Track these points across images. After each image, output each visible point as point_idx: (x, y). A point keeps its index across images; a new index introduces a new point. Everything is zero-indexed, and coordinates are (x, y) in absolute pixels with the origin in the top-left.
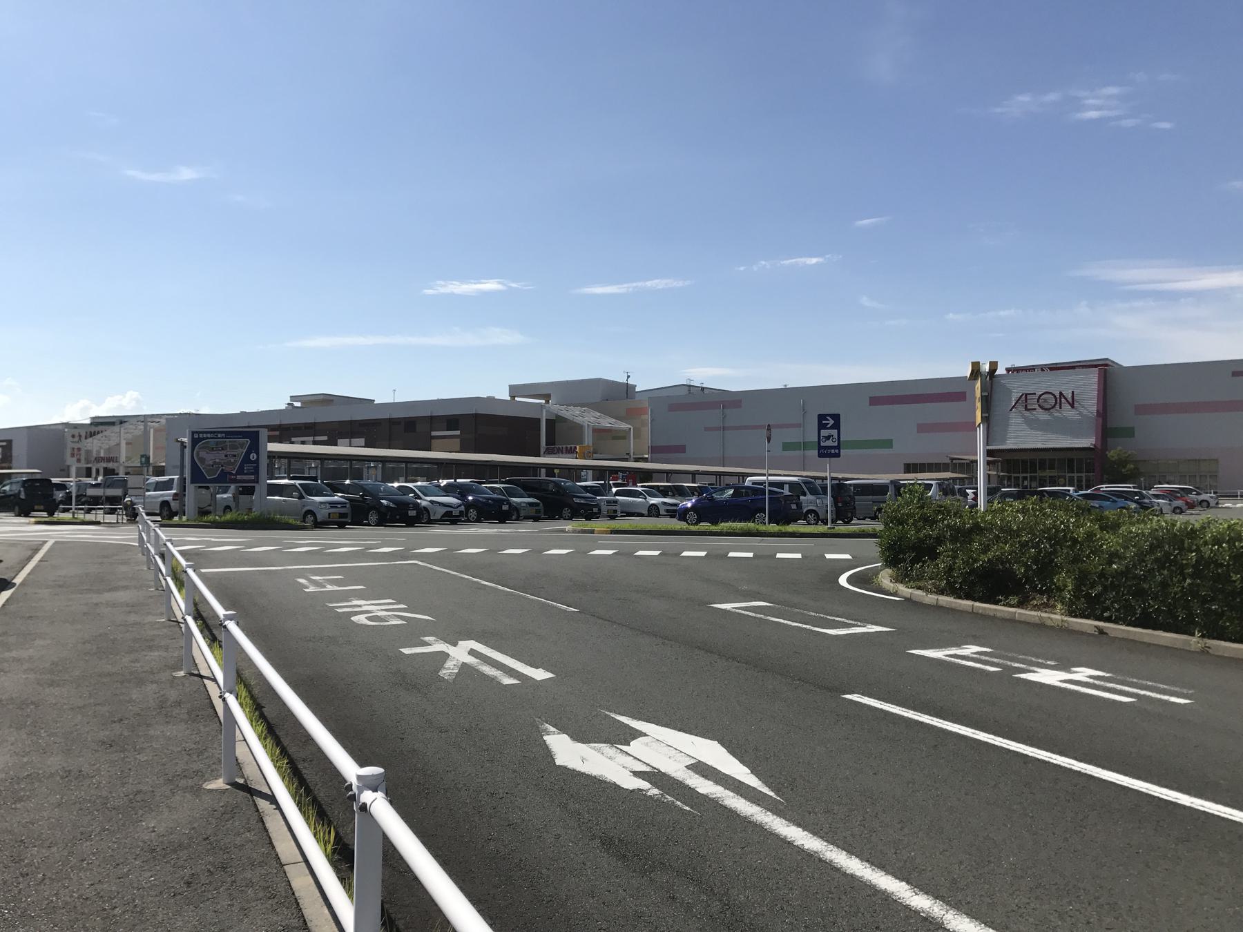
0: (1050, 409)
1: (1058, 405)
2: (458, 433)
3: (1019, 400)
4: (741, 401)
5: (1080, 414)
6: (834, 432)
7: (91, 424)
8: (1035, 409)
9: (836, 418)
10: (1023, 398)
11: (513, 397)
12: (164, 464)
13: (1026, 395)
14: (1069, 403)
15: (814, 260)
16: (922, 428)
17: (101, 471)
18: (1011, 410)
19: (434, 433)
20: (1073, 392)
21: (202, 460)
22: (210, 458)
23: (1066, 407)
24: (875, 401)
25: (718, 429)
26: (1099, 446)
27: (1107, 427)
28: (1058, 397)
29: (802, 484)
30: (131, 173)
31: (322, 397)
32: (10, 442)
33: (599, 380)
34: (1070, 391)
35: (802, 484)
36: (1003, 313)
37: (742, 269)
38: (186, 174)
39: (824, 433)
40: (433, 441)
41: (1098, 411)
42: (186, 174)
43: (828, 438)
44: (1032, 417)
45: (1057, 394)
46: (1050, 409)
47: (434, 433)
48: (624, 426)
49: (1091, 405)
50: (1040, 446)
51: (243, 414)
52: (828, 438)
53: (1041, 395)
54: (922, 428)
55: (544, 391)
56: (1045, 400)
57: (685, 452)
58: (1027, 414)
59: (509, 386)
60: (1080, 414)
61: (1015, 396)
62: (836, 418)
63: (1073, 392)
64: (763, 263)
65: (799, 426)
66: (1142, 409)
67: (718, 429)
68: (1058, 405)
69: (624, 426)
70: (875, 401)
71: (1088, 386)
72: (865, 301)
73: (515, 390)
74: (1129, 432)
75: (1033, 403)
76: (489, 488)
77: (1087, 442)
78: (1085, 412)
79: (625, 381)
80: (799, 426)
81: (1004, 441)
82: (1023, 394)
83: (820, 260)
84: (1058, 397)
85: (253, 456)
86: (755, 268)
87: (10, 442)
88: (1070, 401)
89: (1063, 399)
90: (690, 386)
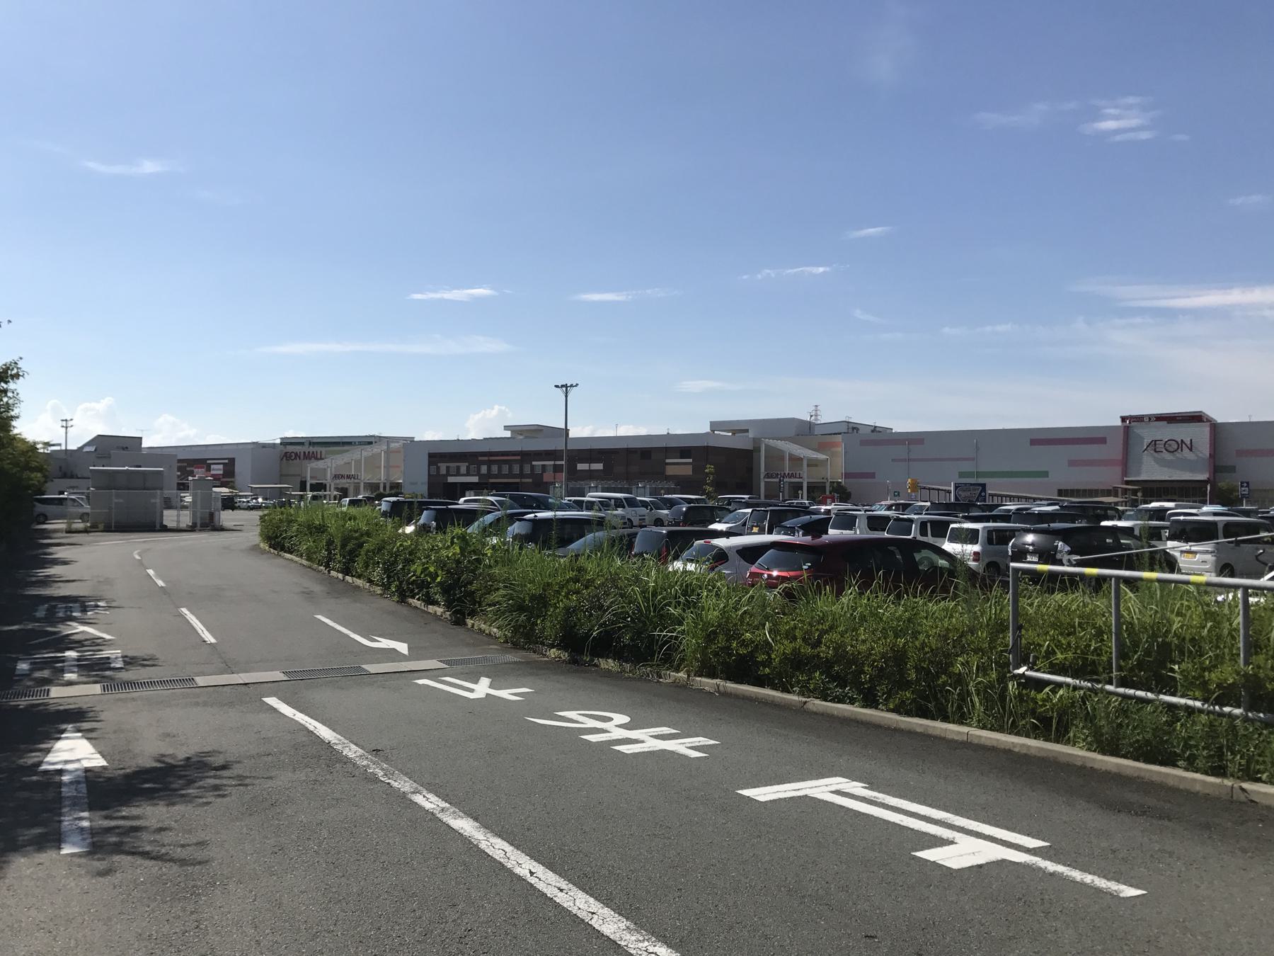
0: (1173, 452)
1: (1180, 449)
2: (691, 460)
3: (1150, 444)
4: (923, 439)
5: (1197, 456)
6: (1247, 489)
7: (281, 444)
8: (1162, 452)
9: (1248, 483)
10: (1154, 442)
11: (713, 431)
12: (401, 481)
13: (1156, 441)
14: (1188, 447)
15: (821, 269)
16: (1072, 463)
17: (328, 488)
18: (1144, 451)
19: (668, 461)
20: (1191, 440)
21: (960, 495)
22: (963, 494)
23: (1186, 450)
24: (1034, 442)
25: (914, 460)
26: (1212, 478)
27: (1218, 467)
28: (1180, 442)
29: (624, 500)
30: (91, 165)
31: (536, 427)
32: (232, 461)
33: (793, 420)
34: (1189, 440)
35: (624, 500)
36: (1000, 328)
37: (745, 277)
38: (149, 167)
39: (1243, 489)
40: (667, 466)
41: (1210, 454)
42: (149, 167)
43: (1244, 491)
44: (1159, 457)
45: (1179, 441)
46: (1173, 452)
47: (668, 461)
48: (822, 457)
49: (1204, 449)
50: (1167, 478)
51: (458, 442)
52: (1244, 491)
53: (1166, 442)
54: (1072, 463)
55: (738, 429)
56: (1170, 445)
57: (874, 478)
58: (1156, 454)
59: (711, 422)
60: (1197, 456)
61: (1146, 441)
62: (1248, 483)
63: (1191, 440)
64: (768, 271)
65: (973, 459)
66: (1241, 453)
67: (914, 460)
68: (1180, 449)
69: (822, 457)
70: (1034, 442)
71: (1200, 435)
72: (858, 313)
73: (715, 425)
74: (1232, 469)
75: (1160, 447)
76: (575, 501)
77: (1203, 476)
78: (1200, 455)
79: (809, 420)
80: (973, 459)
81: (1139, 474)
82: (1152, 442)
83: (828, 269)
84: (1180, 442)
85: (983, 494)
86: (759, 276)
87: (232, 461)
88: (1189, 446)
89: (1184, 445)
90: (848, 422)
